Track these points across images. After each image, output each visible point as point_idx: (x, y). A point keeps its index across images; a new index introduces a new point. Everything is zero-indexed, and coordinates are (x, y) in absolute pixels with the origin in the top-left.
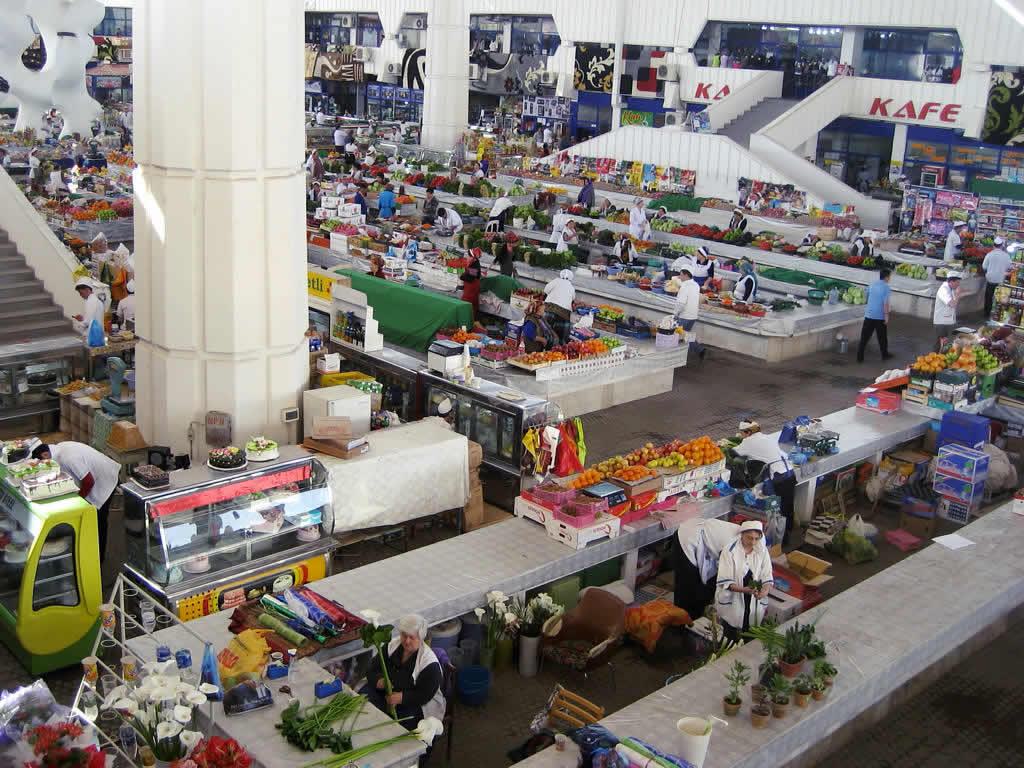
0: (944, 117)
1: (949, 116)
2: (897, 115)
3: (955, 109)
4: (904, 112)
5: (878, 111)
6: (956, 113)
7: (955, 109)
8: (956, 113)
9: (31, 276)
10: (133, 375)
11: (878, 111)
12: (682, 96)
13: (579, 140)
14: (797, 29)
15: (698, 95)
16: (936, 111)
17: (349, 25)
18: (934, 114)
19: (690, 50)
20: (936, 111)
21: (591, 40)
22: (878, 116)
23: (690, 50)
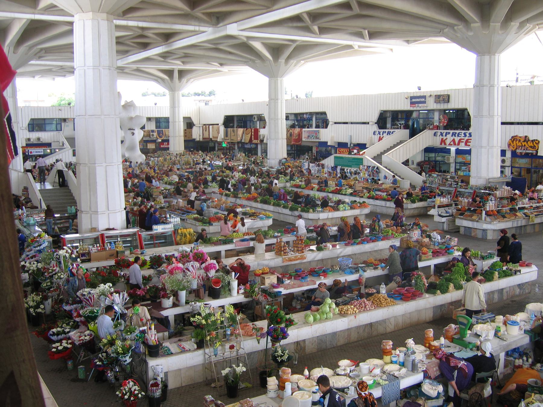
0: (466, 144)
1: (468, 144)
2: (450, 144)
3: (470, 141)
4: (452, 143)
5: (443, 144)
6: (470, 142)
7: (470, 141)
8: (470, 142)
9: (72, 195)
10: (439, 295)
11: (443, 144)
12: (352, 141)
13: (323, 159)
14: (426, 112)
15: (441, 144)
16: (463, 142)
17: (256, 120)
18: (462, 143)
19: (376, 123)
20: (463, 142)
21: (157, 116)
22: (443, 146)
23: (376, 123)
